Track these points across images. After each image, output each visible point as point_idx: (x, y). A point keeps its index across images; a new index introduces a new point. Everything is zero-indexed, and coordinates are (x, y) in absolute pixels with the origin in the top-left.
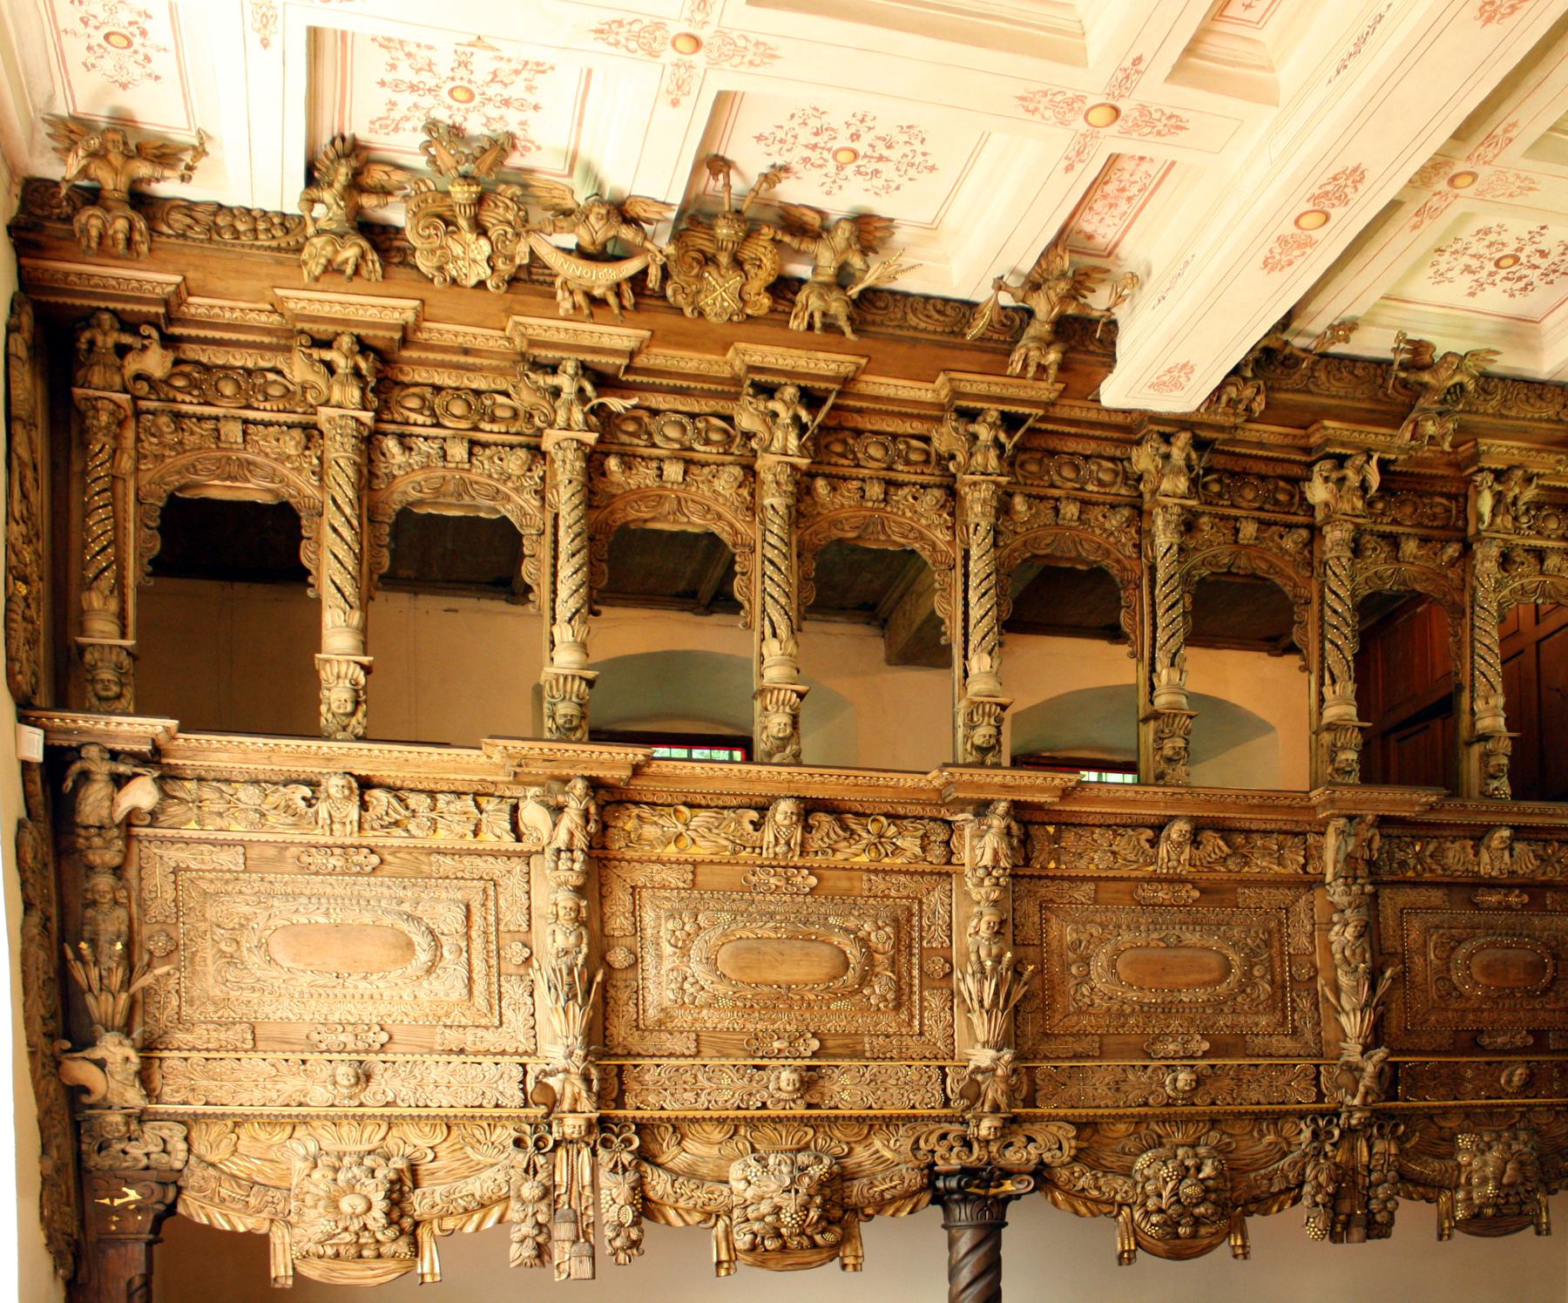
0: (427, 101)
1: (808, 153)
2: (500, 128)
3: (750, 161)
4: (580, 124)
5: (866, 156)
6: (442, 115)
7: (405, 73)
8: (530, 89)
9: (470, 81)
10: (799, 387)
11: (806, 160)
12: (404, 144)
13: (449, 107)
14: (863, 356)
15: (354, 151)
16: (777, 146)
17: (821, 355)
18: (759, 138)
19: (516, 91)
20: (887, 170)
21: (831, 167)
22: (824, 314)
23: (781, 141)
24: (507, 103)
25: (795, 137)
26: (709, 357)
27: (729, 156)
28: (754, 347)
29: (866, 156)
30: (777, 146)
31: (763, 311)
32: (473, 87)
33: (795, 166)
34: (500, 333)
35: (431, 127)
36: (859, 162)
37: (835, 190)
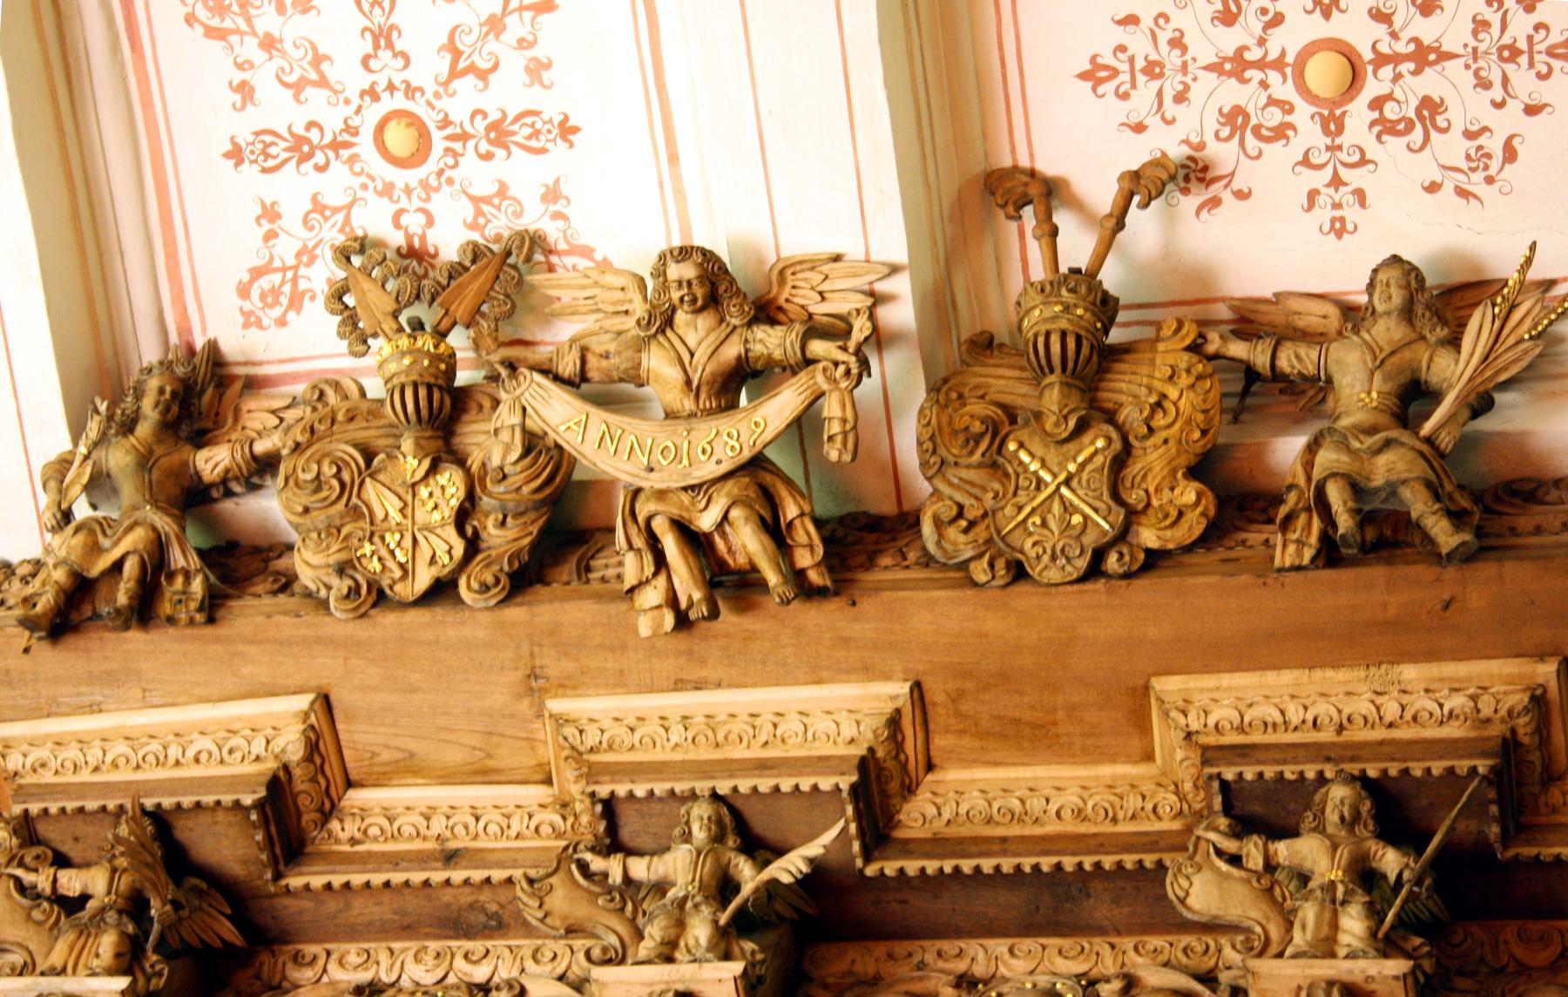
0: (336, 184)
1: (1232, 93)
2: (500, 225)
3: (1079, 139)
4: (673, 158)
5: (1381, 60)
6: (375, 221)
7: (279, 111)
8: (537, 70)
9: (411, 91)
10: (1363, 780)
11: (1235, 119)
12: (296, 343)
13: (387, 191)
14: (1541, 657)
15: (202, 392)
16: (1146, 91)
17: (1410, 673)
18: (1095, 74)
19: (508, 93)
20: (1465, 103)
21: (1308, 134)
22: (1357, 489)
23: (1153, 70)
24: (499, 133)
25: (1177, 43)
26: (1107, 771)
27: (1048, 166)
28: (1209, 681)
29: (1381, 60)
30: (1146, 91)
31: (1194, 525)
32: (418, 108)
33: (1222, 154)
34: (540, 793)
35: (355, 248)
36: (1373, 87)
37: (1352, 213)
